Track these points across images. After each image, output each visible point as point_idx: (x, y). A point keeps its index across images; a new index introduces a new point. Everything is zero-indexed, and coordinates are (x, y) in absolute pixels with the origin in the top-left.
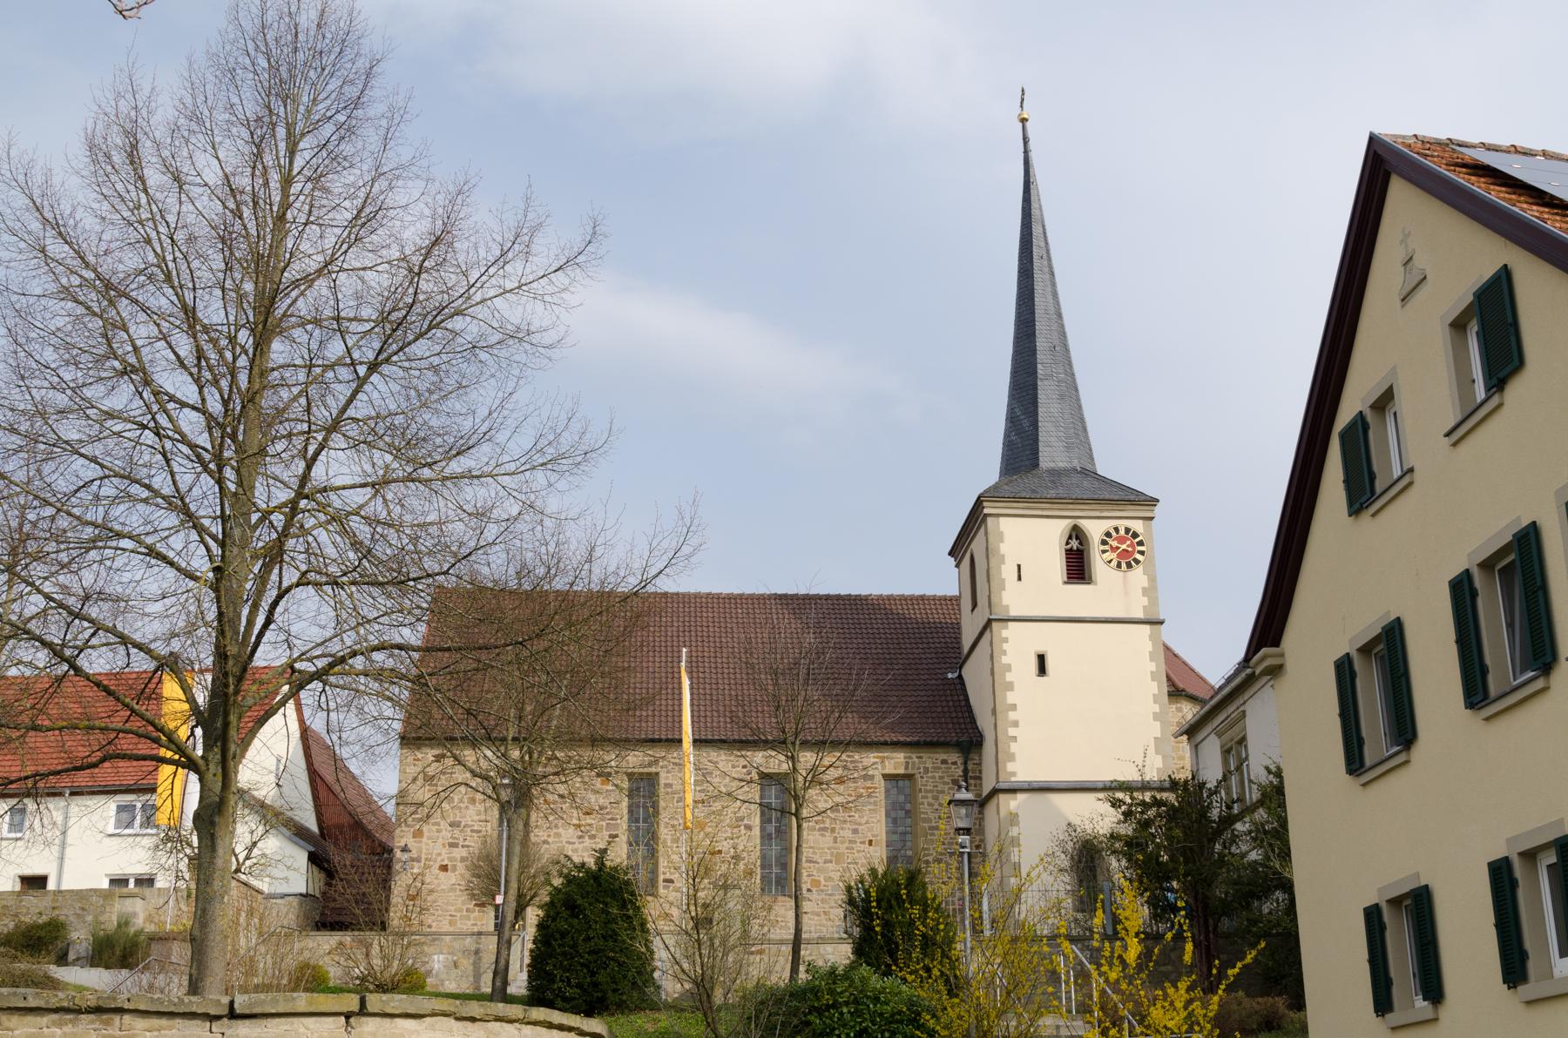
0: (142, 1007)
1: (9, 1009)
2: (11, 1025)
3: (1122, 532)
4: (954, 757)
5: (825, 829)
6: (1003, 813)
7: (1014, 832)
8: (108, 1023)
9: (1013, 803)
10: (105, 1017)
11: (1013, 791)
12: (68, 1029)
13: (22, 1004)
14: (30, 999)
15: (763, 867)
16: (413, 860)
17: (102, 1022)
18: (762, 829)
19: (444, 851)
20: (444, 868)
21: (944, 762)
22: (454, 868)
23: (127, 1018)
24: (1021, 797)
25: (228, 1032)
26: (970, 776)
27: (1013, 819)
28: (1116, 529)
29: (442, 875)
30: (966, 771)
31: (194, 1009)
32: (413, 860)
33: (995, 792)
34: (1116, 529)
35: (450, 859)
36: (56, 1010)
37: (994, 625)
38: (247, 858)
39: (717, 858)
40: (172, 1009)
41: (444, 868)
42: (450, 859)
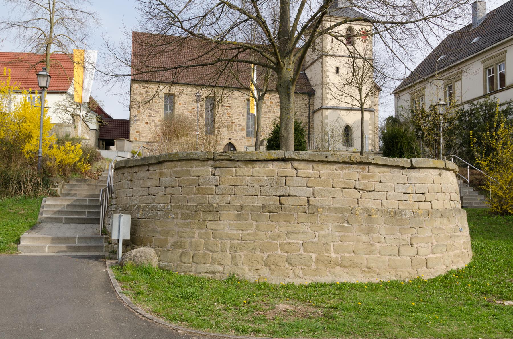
0: (379, 163)
1: (319, 161)
2: (319, 169)
3: (364, 30)
4: (306, 98)
5: (266, 117)
6: (324, 116)
7: (326, 121)
8: (363, 169)
9: (327, 113)
10: (362, 166)
11: (327, 109)
12: (346, 171)
13: (326, 159)
14: (329, 157)
15: (247, 128)
16: (137, 120)
17: (361, 168)
18: (247, 117)
19: (147, 118)
20: (147, 123)
21: (303, 99)
22: (150, 123)
23: (371, 167)
24: (329, 111)
25: (408, 175)
26: (310, 105)
27: (327, 117)
28: (362, 29)
29: (146, 125)
30: (309, 102)
31: (399, 164)
32: (137, 120)
33: (321, 109)
34: (362, 29)
35: (149, 120)
36: (339, 163)
37: (324, 57)
38: (86, 116)
39: (234, 125)
40: (391, 164)
41: (147, 123)
42: (149, 120)
